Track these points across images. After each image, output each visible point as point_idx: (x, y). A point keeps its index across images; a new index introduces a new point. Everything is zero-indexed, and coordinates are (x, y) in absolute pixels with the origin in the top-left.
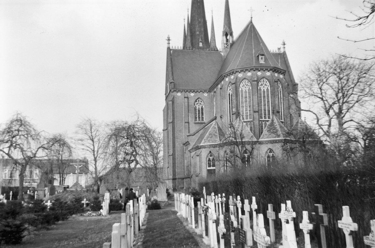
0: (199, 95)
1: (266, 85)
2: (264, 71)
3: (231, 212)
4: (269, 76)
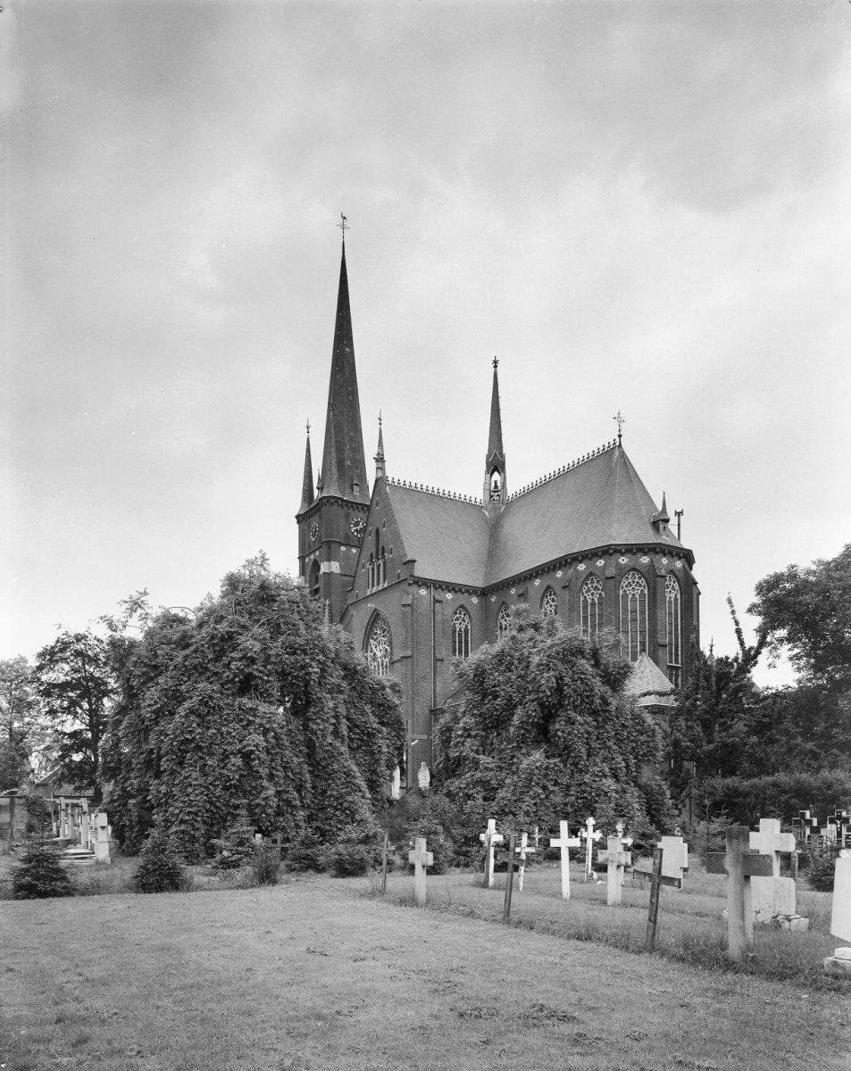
0: (439, 595)
1: (673, 588)
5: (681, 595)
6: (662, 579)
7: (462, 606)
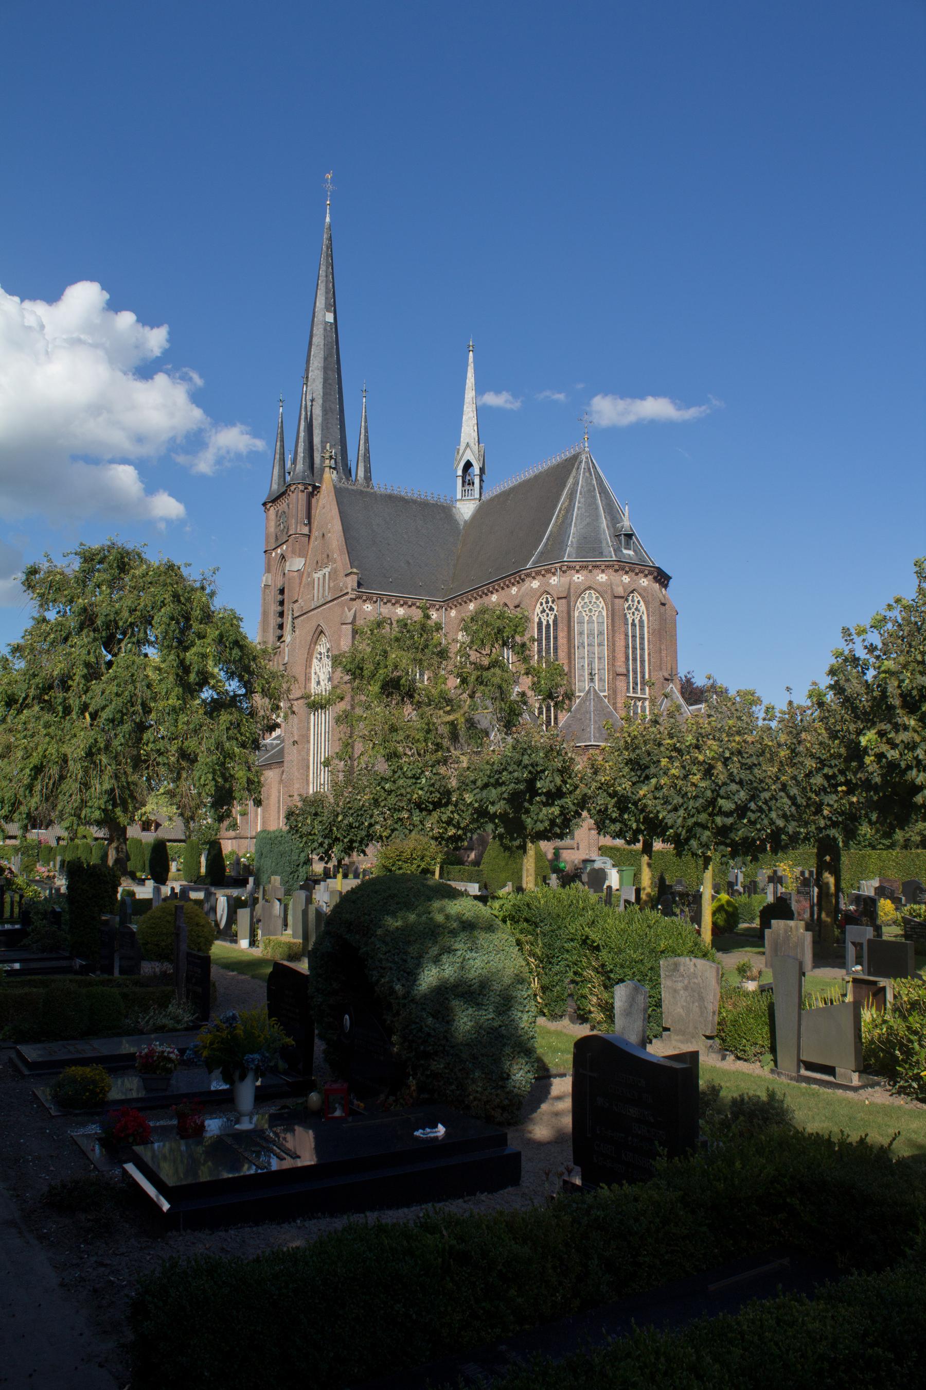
2: (637, 574)
5: (648, 616)
6: (621, 601)
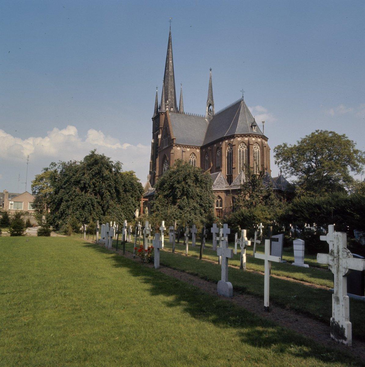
0: (184, 149)
1: (257, 148)
3: (169, 250)
4: (260, 142)
5: (260, 150)
7: (193, 153)
